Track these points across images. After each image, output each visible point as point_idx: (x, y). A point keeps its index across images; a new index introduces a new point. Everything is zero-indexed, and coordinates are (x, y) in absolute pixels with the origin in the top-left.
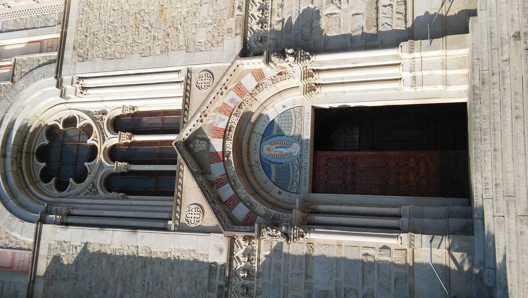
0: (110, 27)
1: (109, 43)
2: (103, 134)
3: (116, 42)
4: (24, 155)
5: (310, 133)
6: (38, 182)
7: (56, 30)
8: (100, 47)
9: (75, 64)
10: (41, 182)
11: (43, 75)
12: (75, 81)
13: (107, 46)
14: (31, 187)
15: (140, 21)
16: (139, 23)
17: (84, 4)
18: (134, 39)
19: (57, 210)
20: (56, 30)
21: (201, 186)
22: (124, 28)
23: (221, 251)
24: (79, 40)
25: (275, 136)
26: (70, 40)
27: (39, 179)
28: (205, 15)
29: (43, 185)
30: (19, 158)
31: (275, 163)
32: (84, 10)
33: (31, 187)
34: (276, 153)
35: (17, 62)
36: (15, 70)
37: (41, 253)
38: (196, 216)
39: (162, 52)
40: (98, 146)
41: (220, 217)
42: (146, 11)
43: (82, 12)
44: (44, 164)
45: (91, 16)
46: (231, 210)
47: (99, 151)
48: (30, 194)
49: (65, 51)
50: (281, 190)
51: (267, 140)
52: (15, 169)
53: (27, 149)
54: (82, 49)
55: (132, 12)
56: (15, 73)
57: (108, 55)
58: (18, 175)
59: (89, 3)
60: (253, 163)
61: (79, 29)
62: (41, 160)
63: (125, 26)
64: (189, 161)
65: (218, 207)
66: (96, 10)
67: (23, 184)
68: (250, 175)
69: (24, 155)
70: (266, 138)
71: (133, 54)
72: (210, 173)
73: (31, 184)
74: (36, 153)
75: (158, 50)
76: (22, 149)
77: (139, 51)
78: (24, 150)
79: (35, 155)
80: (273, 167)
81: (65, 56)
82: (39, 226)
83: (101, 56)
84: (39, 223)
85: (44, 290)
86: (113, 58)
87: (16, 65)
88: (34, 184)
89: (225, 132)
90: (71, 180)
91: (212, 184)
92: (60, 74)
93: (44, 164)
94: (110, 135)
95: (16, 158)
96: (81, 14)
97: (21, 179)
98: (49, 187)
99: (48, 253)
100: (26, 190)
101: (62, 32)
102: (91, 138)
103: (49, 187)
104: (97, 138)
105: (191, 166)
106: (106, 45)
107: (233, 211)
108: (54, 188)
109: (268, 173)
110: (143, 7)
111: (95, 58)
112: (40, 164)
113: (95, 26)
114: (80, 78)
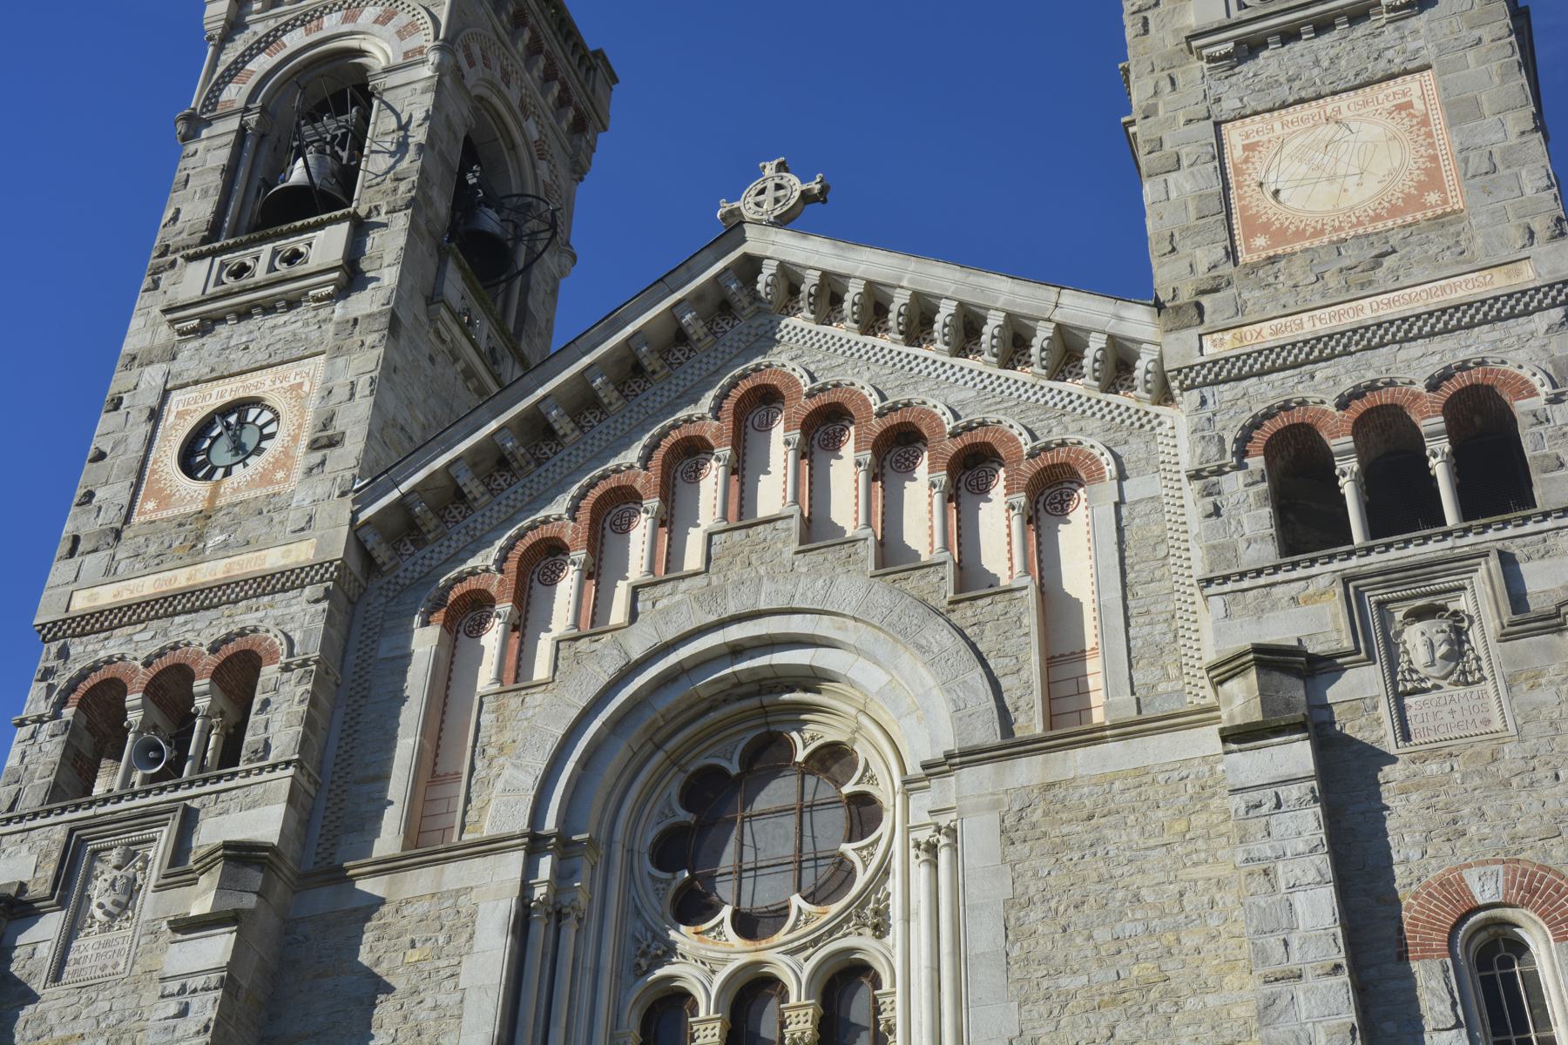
0: (1120, 895)
1: (1062, 909)
2: (815, 942)
3: (1065, 931)
7: (1117, 699)
8: (1051, 880)
9: (996, 805)
10: (683, 777)
11: (962, 706)
12: (944, 821)
13: (1053, 904)
15: (1136, 1003)
16: (1129, 1003)
17: (1207, 774)
18: (1075, 996)
19: (572, 874)
20: (1117, 699)
22: (1113, 950)
24: (1076, 796)
27: (692, 769)
29: (675, 789)
32: (1182, 785)
33: (659, 757)
35: (1018, 594)
36: (988, 600)
37: (450, 868)
40: (780, 937)
42: (1174, 1022)
43: (1175, 776)
45: (1160, 813)
48: (635, 762)
49: (1040, 757)
54: (1046, 814)
55: (1170, 966)
56: (980, 602)
57: (1022, 914)
58: (690, 707)
59: (1208, 792)
61: (1117, 784)
63: (1119, 952)
66: (1180, 826)
67: (663, 733)
69: (754, 702)
71: (1020, 1006)
77: (1030, 1025)
78: (767, 700)
79: (763, 730)
81: (1024, 761)
82: (518, 841)
83: (1019, 890)
84: (526, 840)
85: (356, 910)
86: (1010, 937)
87: (1007, 596)
88: (674, 761)
92: (963, 765)
94: (808, 967)
96: (1167, 775)
98: (667, 811)
99: (448, 891)
100: (650, 746)
102: (806, 906)
103: (667, 811)
104: (806, 923)
106: (1057, 899)
108: (661, 827)
110: (1190, 1004)
111: (1013, 870)
112: (736, 758)
113: (1124, 838)
114: (952, 832)
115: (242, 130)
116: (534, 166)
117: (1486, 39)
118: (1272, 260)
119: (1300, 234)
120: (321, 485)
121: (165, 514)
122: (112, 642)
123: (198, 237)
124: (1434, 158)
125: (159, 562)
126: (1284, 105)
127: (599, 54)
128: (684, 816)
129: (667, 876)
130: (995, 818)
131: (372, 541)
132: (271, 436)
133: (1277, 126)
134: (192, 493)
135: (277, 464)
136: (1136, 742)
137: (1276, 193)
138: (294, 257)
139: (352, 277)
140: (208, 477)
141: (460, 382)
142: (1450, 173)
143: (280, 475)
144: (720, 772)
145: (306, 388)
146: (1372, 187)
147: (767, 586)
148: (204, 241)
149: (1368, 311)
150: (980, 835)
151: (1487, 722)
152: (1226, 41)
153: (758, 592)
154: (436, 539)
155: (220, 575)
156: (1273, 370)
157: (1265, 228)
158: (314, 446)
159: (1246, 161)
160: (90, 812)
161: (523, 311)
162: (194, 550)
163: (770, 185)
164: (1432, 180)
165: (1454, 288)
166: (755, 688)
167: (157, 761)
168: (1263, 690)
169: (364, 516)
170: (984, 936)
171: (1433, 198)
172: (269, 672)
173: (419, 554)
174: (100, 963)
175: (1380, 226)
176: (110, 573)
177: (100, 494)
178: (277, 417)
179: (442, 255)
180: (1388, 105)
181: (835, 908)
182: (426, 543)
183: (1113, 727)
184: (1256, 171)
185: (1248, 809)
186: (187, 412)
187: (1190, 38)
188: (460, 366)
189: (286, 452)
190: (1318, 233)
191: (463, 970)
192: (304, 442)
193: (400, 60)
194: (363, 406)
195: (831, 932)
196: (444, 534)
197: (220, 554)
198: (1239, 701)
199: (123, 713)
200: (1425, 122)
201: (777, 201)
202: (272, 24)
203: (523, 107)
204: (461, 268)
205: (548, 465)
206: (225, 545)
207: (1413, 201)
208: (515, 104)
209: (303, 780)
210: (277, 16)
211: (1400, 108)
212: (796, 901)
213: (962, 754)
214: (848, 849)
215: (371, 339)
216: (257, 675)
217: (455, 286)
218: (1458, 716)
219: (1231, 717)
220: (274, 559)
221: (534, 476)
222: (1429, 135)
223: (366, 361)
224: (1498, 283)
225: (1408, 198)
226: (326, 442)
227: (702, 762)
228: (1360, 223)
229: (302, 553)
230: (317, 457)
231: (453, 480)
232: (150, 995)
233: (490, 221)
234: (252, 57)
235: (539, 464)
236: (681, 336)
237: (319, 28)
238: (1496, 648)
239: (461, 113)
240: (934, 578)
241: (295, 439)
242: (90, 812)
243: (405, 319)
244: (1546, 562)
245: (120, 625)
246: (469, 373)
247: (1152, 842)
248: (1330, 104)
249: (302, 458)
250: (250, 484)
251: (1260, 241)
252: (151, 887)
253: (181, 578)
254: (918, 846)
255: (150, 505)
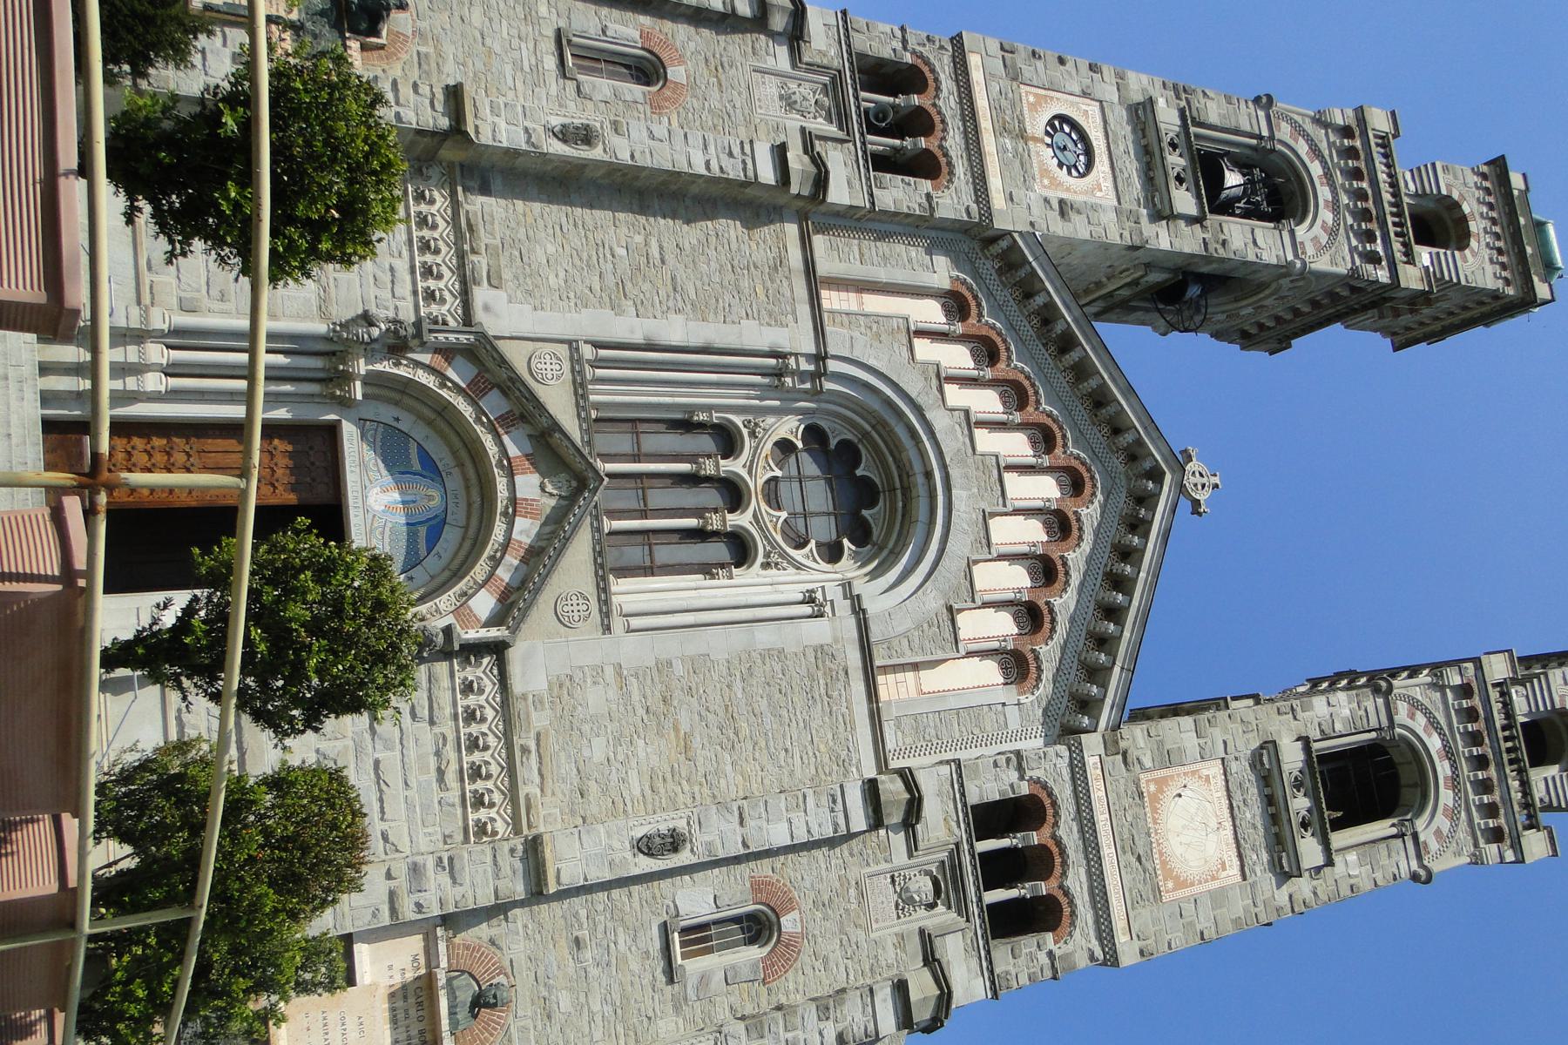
4: (898, 484)
5: (353, 529)
6: (860, 440)
9: (836, 640)
12: (828, 609)
14: (868, 428)
21: (540, 406)
23: (487, 308)
25: (420, 523)
26: (858, 687)
27: (860, 446)
28: (595, 741)
29: (849, 436)
30: (905, 476)
31: (415, 474)
33: (868, 428)
34: (415, 491)
37: (807, 308)
38: (544, 366)
39: (670, 664)
40: (764, 506)
41: (495, 355)
44: (859, 472)
46: (478, 374)
47: (760, 497)
48: (865, 413)
50: (394, 424)
51: (436, 516)
52: (904, 455)
53: (895, 495)
60: (456, 471)
62: (866, 482)
64: (572, 451)
65: (504, 374)
68: (458, 444)
69: (898, 484)
70: (438, 520)
72: (530, 436)
73: (868, 433)
74: (878, 493)
75: (679, 668)
76: (903, 494)
78: (899, 493)
80: (417, 466)
88: (866, 435)
89: (515, 511)
90: (800, 445)
91: (523, 418)
93: (859, 472)
95: (908, 476)
97: (888, 439)
100: (874, 422)
101: (877, 702)
105: (565, 443)
107: (476, 371)
109: (424, 456)
115: (1260, 137)
116: (1223, 312)
117: (1257, 910)
118: (1141, 795)
119: (1155, 810)
120: (1038, 210)
121: (1026, 109)
122: (949, 82)
123: (1195, 114)
124: (1192, 884)
125: (996, 109)
126: (1229, 797)
127: (1289, 346)
128: (833, 443)
129: (799, 436)
130: (829, 640)
131: (1004, 244)
132: (1070, 173)
133: (1219, 794)
134: (1037, 124)
135: (1053, 179)
136: (867, 721)
137: (1180, 796)
138: (1180, 180)
139: (1162, 213)
140: (1047, 133)
141: (1094, 279)
142: (1180, 894)
143: (1046, 182)
144: (857, 463)
145: (1099, 194)
146: (1178, 850)
147: (964, 494)
148: (1193, 119)
149: (1108, 851)
150: (818, 631)
151: (877, 921)
152: (1270, 763)
153: (962, 489)
154: (1002, 282)
155: (983, 126)
156: (1077, 803)
157: (1160, 790)
158: (1062, 202)
159: (1200, 777)
160: (849, 81)
161: (1135, 309)
162: (1002, 129)
163: (1205, 480)
164: (1181, 884)
165: (1109, 845)
166: (906, 485)
167: (877, 119)
168: (898, 802)
169: (1016, 236)
170: (765, 636)
171: (1170, 885)
172: (926, 185)
173: (993, 272)
174: (762, 97)
175: (1156, 856)
176: (988, 77)
177: (1040, 64)
178: (1082, 176)
179: (1175, 270)
180: (1225, 857)
181: (779, 538)
182: (1000, 276)
183: (878, 708)
184: (1194, 784)
185: (832, 796)
186: (1087, 117)
187: (1274, 742)
188: (1104, 280)
189: (1060, 184)
190: (1155, 821)
191: (752, 322)
192: (1064, 196)
193: (1298, 240)
194: (1083, 233)
195: (766, 537)
196: (1005, 286)
197: (1000, 148)
198: (891, 787)
199: (906, 92)
200: (1214, 878)
201: (1195, 485)
202: (1326, 153)
203: (1262, 307)
204: (1166, 281)
205: (1044, 351)
206: (1005, 151)
207: (1169, 874)
208: (1266, 303)
209: (863, 213)
210: (1331, 156)
211: (1223, 864)
212: (784, 515)
213: (865, 619)
214: (812, 544)
215: (1126, 234)
216: (926, 178)
217: (1155, 277)
218: (880, 906)
219: (883, 782)
220: (995, 183)
221: (1037, 342)
222: (1206, 881)
223: (1114, 232)
224: (1119, 923)
225: (1171, 870)
226: (1064, 208)
227: (863, 452)
228: (1159, 844)
229: (998, 201)
230: (1056, 205)
231: (1039, 292)
232: (743, 133)
233: (1194, 291)
234: (1307, 141)
235: (1045, 345)
236: (1116, 431)
237: (1322, 184)
238: (916, 926)
239: (1264, 276)
240: (968, 600)
241: (1068, 190)
242: (849, 81)
243: (1137, 253)
244: (963, 951)
245: (958, 85)
246: (1099, 285)
247: (814, 732)
248: (1228, 824)
249: (1055, 195)
250: (1041, 163)
251: (1152, 788)
252: (804, 124)
253: (985, 124)
254: (812, 591)
255: (1031, 99)
